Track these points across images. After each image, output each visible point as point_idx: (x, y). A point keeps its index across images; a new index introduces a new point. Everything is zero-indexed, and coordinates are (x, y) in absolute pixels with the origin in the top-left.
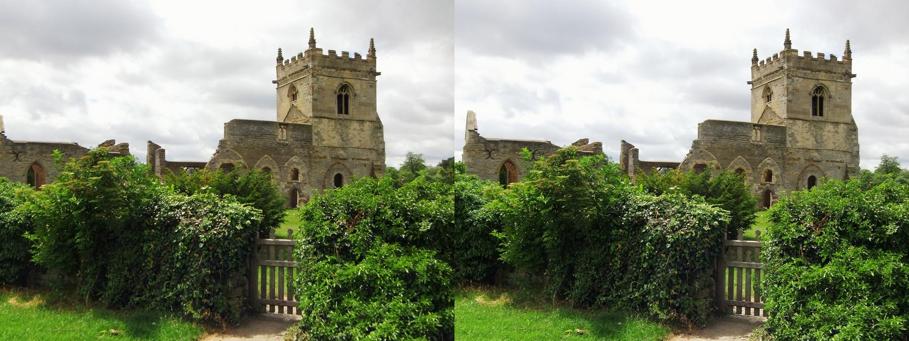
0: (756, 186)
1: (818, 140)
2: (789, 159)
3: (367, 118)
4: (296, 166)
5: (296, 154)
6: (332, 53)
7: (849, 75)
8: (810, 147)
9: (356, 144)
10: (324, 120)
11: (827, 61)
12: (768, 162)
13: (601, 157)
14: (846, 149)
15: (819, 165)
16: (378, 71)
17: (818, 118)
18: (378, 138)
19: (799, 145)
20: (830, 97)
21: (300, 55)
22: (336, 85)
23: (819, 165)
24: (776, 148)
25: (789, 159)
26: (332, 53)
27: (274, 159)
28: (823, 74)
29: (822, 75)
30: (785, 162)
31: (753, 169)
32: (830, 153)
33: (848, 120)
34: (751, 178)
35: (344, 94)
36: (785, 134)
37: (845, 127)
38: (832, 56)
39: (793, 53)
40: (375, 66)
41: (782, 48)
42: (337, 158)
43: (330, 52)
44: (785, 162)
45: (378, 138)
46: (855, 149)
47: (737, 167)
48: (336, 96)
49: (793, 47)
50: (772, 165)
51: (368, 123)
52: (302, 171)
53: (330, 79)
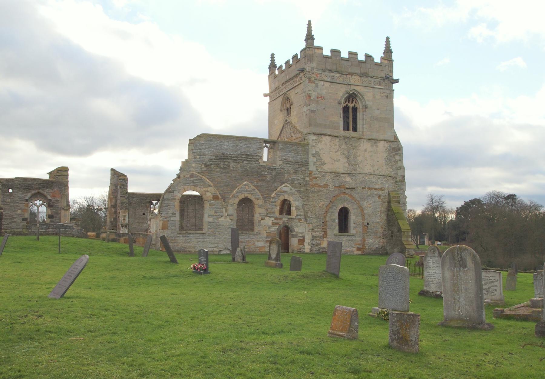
0: (268, 221)
1: (352, 161)
2: (313, 186)
3: (381, 137)
4: (286, 197)
5: (287, 181)
6: (336, 53)
7: (391, 81)
8: (342, 171)
9: (367, 169)
10: (324, 138)
11: (360, 62)
12: (285, 189)
13: (66, 174)
14: (387, 173)
15: (354, 194)
16: (395, 77)
17: (351, 133)
18: (396, 161)
19: (326, 168)
20: (366, 108)
21: (295, 57)
22: (341, 94)
23: (354, 194)
24: (296, 172)
25: (313, 186)
26: (336, 53)
27: (256, 187)
28: (357, 78)
29: (355, 80)
30: (305, 190)
31: (264, 198)
32: (367, 178)
33: (390, 137)
34: (262, 211)
35: (351, 105)
36: (307, 153)
37: (386, 145)
38: (368, 56)
39: (316, 51)
40: (392, 72)
41: (303, 45)
42: (341, 187)
43: (333, 51)
44: (305, 190)
45: (396, 161)
46: (400, 173)
47: (242, 196)
48: (341, 107)
49: (316, 43)
50: (289, 194)
51: (382, 142)
52: (296, 204)
53: (333, 86)
